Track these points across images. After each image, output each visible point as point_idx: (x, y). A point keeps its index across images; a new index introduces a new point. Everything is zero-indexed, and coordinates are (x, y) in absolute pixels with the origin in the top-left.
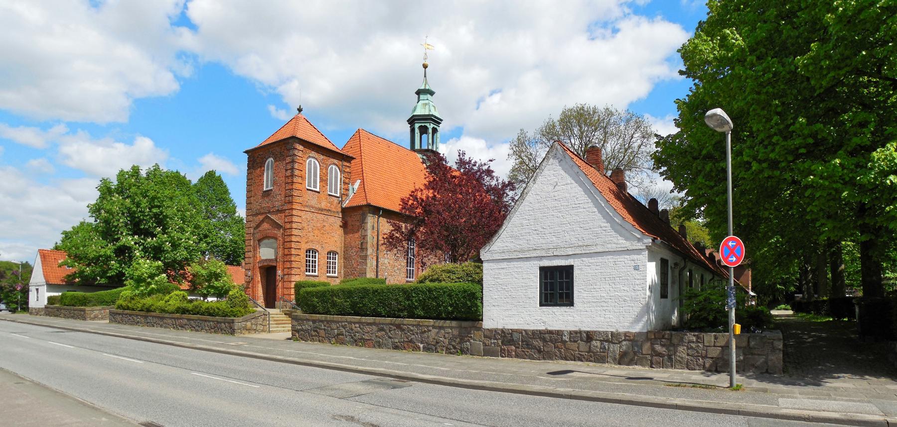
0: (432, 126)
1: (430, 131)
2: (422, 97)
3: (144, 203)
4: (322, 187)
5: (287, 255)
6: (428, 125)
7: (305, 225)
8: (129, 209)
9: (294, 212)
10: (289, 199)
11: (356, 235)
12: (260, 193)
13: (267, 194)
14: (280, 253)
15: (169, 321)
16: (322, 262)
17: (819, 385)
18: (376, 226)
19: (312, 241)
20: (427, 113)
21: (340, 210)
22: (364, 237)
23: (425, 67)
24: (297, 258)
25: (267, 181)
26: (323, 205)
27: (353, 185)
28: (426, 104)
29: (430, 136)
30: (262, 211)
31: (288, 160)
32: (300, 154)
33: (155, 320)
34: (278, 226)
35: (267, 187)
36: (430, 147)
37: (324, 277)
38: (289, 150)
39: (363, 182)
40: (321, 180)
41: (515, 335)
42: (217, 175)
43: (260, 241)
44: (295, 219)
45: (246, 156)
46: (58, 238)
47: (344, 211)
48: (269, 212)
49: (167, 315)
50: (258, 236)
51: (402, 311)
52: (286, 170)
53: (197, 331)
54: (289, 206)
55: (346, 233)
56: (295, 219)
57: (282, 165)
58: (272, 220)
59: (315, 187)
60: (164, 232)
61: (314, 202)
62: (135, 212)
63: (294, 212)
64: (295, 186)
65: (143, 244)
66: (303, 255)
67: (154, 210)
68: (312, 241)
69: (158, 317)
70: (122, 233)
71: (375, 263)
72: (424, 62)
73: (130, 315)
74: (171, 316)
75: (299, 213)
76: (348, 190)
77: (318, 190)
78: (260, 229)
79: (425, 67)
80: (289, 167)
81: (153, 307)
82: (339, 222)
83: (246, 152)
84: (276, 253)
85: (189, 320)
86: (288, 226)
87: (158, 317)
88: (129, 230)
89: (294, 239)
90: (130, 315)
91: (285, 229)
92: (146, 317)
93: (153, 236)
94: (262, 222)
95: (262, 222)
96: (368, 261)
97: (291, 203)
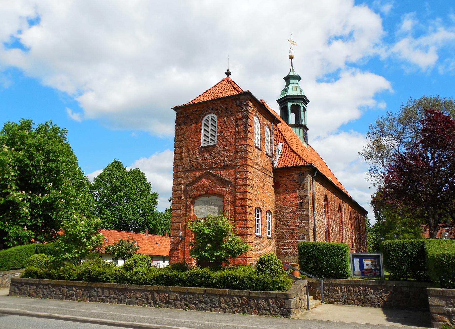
2: (291, 81)
3: (39, 156)
6: (300, 104)
8: (20, 161)
11: (292, 195)
12: (196, 149)
13: (208, 149)
15: (139, 295)
20: (299, 94)
21: (272, 170)
22: (304, 197)
23: (291, 58)
28: (296, 87)
30: (200, 167)
31: (239, 115)
33: (106, 292)
34: (226, 183)
38: (240, 106)
43: (194, 198)
45: (175, 113)
47: (275, 170)
48: (211, 168)
49: (135, 286)
50: (193, 193)
52: (236, 126)
53: (203, 309)
54: (242, 162)
55: (276, 193)
57: (229, 121)
58: (214, 176)
60: (56, 187)
62: (26, 165)
65: (30, 200)
67: (50, 165)
69: (115, 289)
70: (11, 187)
72: (290, 54)
73: (54, 286)
74: (143, 287)
78: (196, 185)
79: (291, 58)
80: (240, 122)
81: (102, 277)
82: (270, 181)
83: (175, 109)
84: (159, 215)
85: (181, 293)
86: (241, 182)
87: (115, 289)
88: (17, 185)
90: (54, 286)
91: (235, 186)
92: (87, 289)
93: (43, 191)
94: (200, 177)
95: (200, 177)
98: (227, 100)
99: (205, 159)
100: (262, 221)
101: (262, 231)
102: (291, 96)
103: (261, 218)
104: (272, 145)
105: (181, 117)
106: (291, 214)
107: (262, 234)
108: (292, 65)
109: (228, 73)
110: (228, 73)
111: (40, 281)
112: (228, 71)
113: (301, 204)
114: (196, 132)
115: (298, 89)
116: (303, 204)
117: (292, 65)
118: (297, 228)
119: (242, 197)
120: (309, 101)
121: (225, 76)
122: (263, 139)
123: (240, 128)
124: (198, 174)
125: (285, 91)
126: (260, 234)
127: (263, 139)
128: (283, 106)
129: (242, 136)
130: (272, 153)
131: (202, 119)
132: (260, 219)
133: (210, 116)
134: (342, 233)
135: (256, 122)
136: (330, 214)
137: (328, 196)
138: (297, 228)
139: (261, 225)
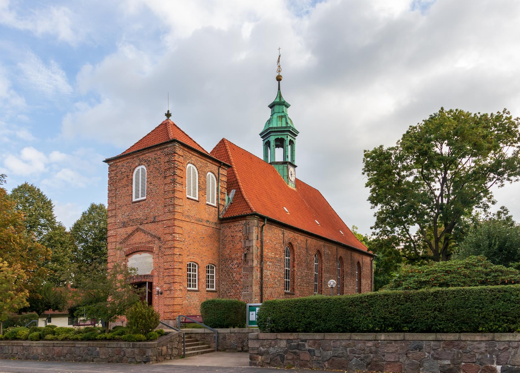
0: (289, 138)
1: (287, 142)
5: (169, 271)
6: (284, 137)
9: (176, 223)
10: (170, 205)
18: (259, 236)
23: (279, 79)
28: (282, 117)
32: (181, 159)
35: (137, 197)
42: (433, 115)
44: (177, 230)
46: (375, 219)
51: (389, 326)
52: (165, 177)
64: (177, 194)
71: (259, 276)
77: (197, 199)
78: (129, 243)
79: (279, 79)
96: (254, 273)
98: (169, 145)
99: (140, 214)
100: (198, 276)
101: (198, 285)
102: (274, 128)
103: (198, 272)
104: (218, 194)
105: (113, 171)
106: (236, 266)
107: (198, 288)
108: (279, 89)
109: (168, 115)
110: (168, 115)
111: (242, 330)
112: (168, 111)
113: (245, 255)
114: (127, 186)
115: (284, 119)
116: (247, 255)
117: (279, 89)
118: (242, 280)
120: (298, 132)
121: (165, 118)
122: (203, 188)
123: (168, 180)
124: (129, 230)
125: (269, 121)
126: (197, 289)
127: (203, 188)
128: (266, 141)
130: (218, 203)
131: (133, 172)
132: (197, 273)
133: (140, 168)
134: (321, 281)
135: (191, 170)
136: (296, 262)
137: (295, 244)
138: (242, 280)
139: (198, 279)
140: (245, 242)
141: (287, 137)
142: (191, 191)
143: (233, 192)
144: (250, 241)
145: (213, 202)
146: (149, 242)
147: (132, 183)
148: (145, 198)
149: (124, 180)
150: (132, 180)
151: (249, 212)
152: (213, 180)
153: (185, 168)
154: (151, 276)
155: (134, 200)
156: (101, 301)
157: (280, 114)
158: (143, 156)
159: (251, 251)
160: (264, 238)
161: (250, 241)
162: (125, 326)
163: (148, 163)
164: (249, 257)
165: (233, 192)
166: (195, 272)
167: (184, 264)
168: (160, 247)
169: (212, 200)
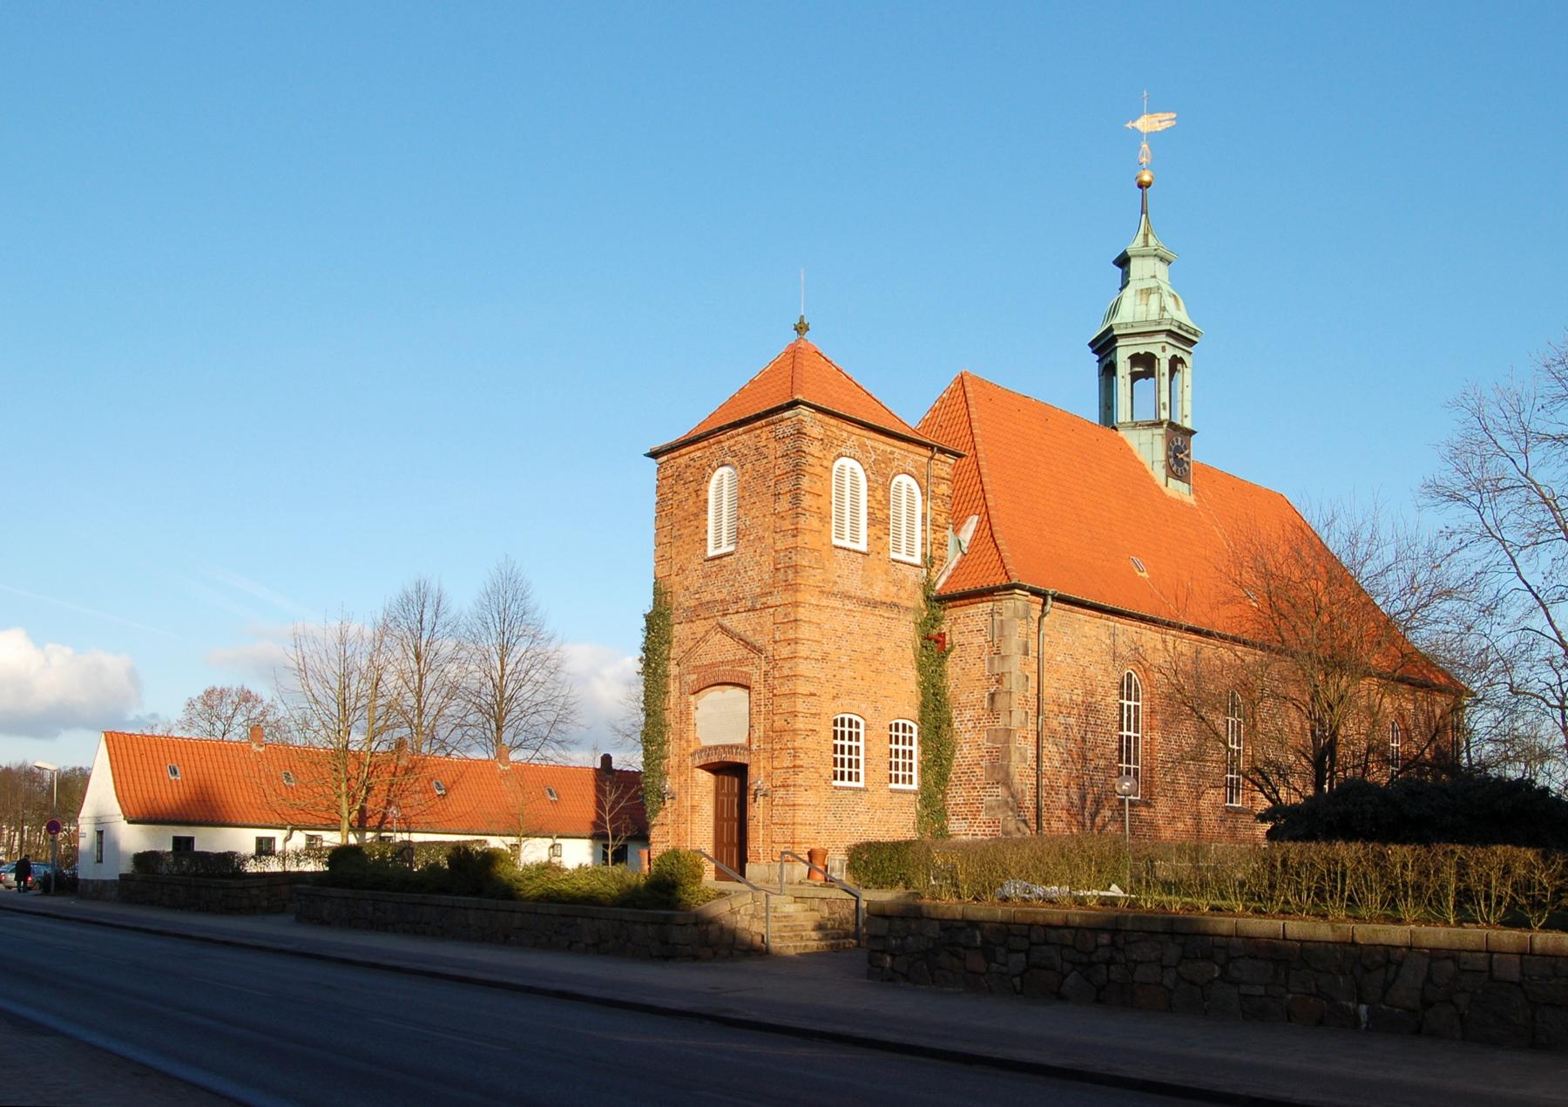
0: (1170, 352)
1: (1164, 366)
4: (874, 539)
5: (778, 735)
7: (829, 647)
10: (787, 574)
14: (759, 733)
16: (875, 752)
17: (849, 849)
19: (849, 693)
24: (810, 742)
25: (719, 529)
26: (878, 591)
27: (956, 531)
29: (1165, 380)
35: (718, 545)
36: (1164, 415)
37: (884, 792)
39: (987, 523)
40: (873, 520)
41: (90, 887)
54: (788, 597)
56: (805, 632)
59: (855, 539)
61: (853, 584)
63: (802, 613)
64: (804, 539)
66: (826, 732)
68: (849, 693)
75: (814, 616)
76: (943, 545)
86: (785, 651)
89: (803, 688)
91: (773, 661)
97: (791, 587)
100: (867, 750)
103: (866, 740)
106: (970, 725)
109: (801, 328)
110: (801, 328)
113: (992, 696)
115: (1154, 298)
119: (785, 689)
121: (793, 336)
127: (879, 521)
129: (787, 525)
135: (848, 474)
140: (991, 661)
141: (1164, 349)
142: (850, 530)
143: (972, 523)
144: (1003, 658)
145: (911, 553)
146: (741, 662)
147: (706, 512)
148: (732, 548)
149: (691, 502)
150: (706, 501)
151: (1001, 580)
152: (910, 491)
153: (828, 469)
154: (748, 748)
155: (711, 553)
156: (1007, 754)
157: (1145, 285)
158: (732, 442)
159: (1006, 685)
160: (1049, 650)
161: (1003, 658)
162: (1167, 834)
163: (739, 460)
164: (1001, 702)
165: (972, 523)
166: (858, 739)
167: (824, 718)
168: (766, 673)
169: (909, 546)
